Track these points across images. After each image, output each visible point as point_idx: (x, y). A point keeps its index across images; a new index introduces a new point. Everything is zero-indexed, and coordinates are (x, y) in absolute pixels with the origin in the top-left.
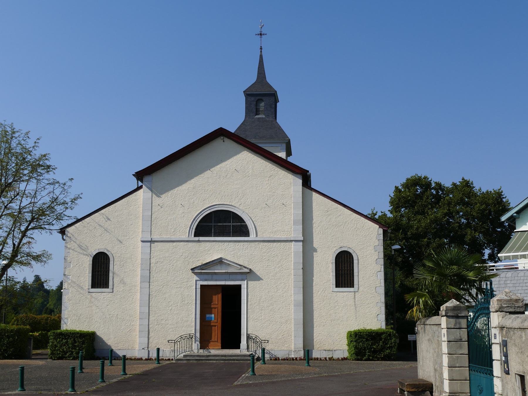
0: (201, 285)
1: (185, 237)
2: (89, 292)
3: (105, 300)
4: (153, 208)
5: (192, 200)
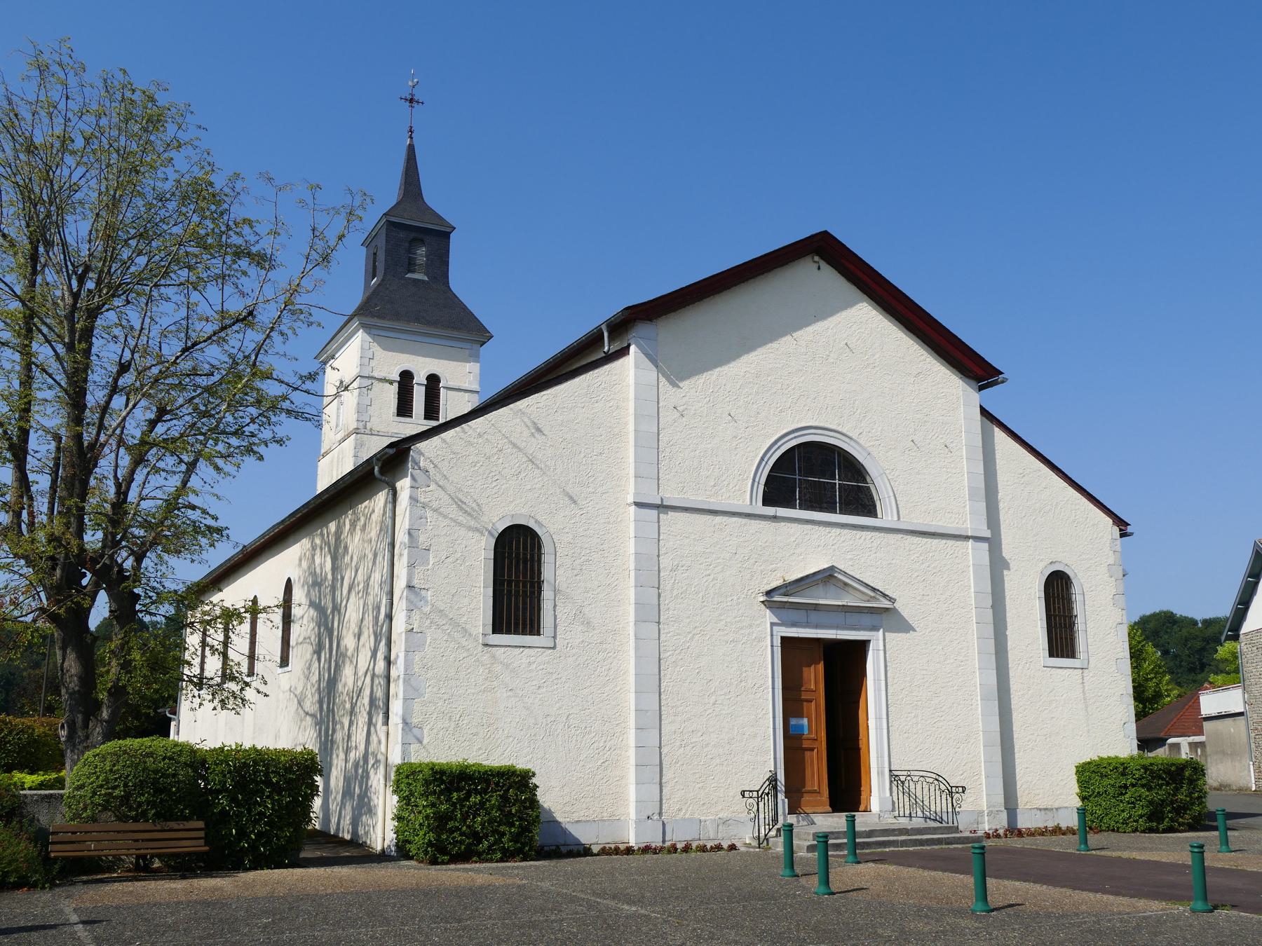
0: (782, 638)
1: (741, 502)
2: (486, 645)
3: (531, 671)
4: (661, 415)
5: (755, 406)
